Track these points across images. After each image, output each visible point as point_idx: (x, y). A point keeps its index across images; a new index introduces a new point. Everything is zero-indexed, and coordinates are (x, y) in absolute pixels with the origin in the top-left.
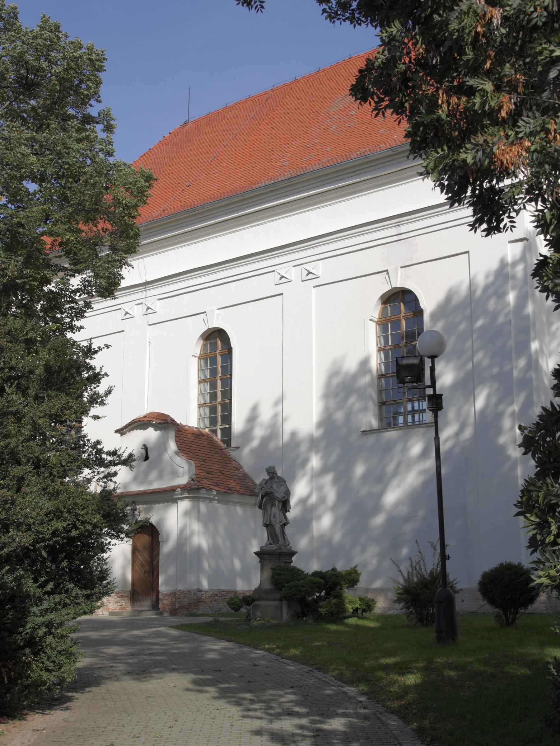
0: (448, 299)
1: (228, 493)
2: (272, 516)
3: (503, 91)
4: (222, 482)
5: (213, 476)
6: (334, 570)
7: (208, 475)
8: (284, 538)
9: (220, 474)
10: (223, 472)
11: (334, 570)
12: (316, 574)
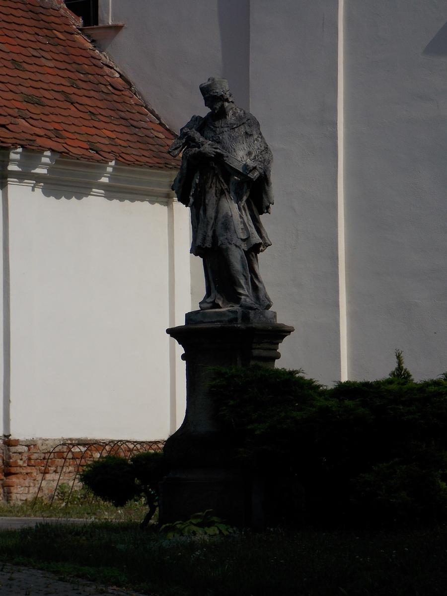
0: (292, 373)
1: (90, 159)
2: (220, 224)
3: (216, 526)
4: (73, 129)
5: (47, 110)
6: (401, 374)
7: (31, 108)
8: (255, 288)
9: (68, 105)
10: (75, 98)
11: (401, 374)
12: (345, 390)
